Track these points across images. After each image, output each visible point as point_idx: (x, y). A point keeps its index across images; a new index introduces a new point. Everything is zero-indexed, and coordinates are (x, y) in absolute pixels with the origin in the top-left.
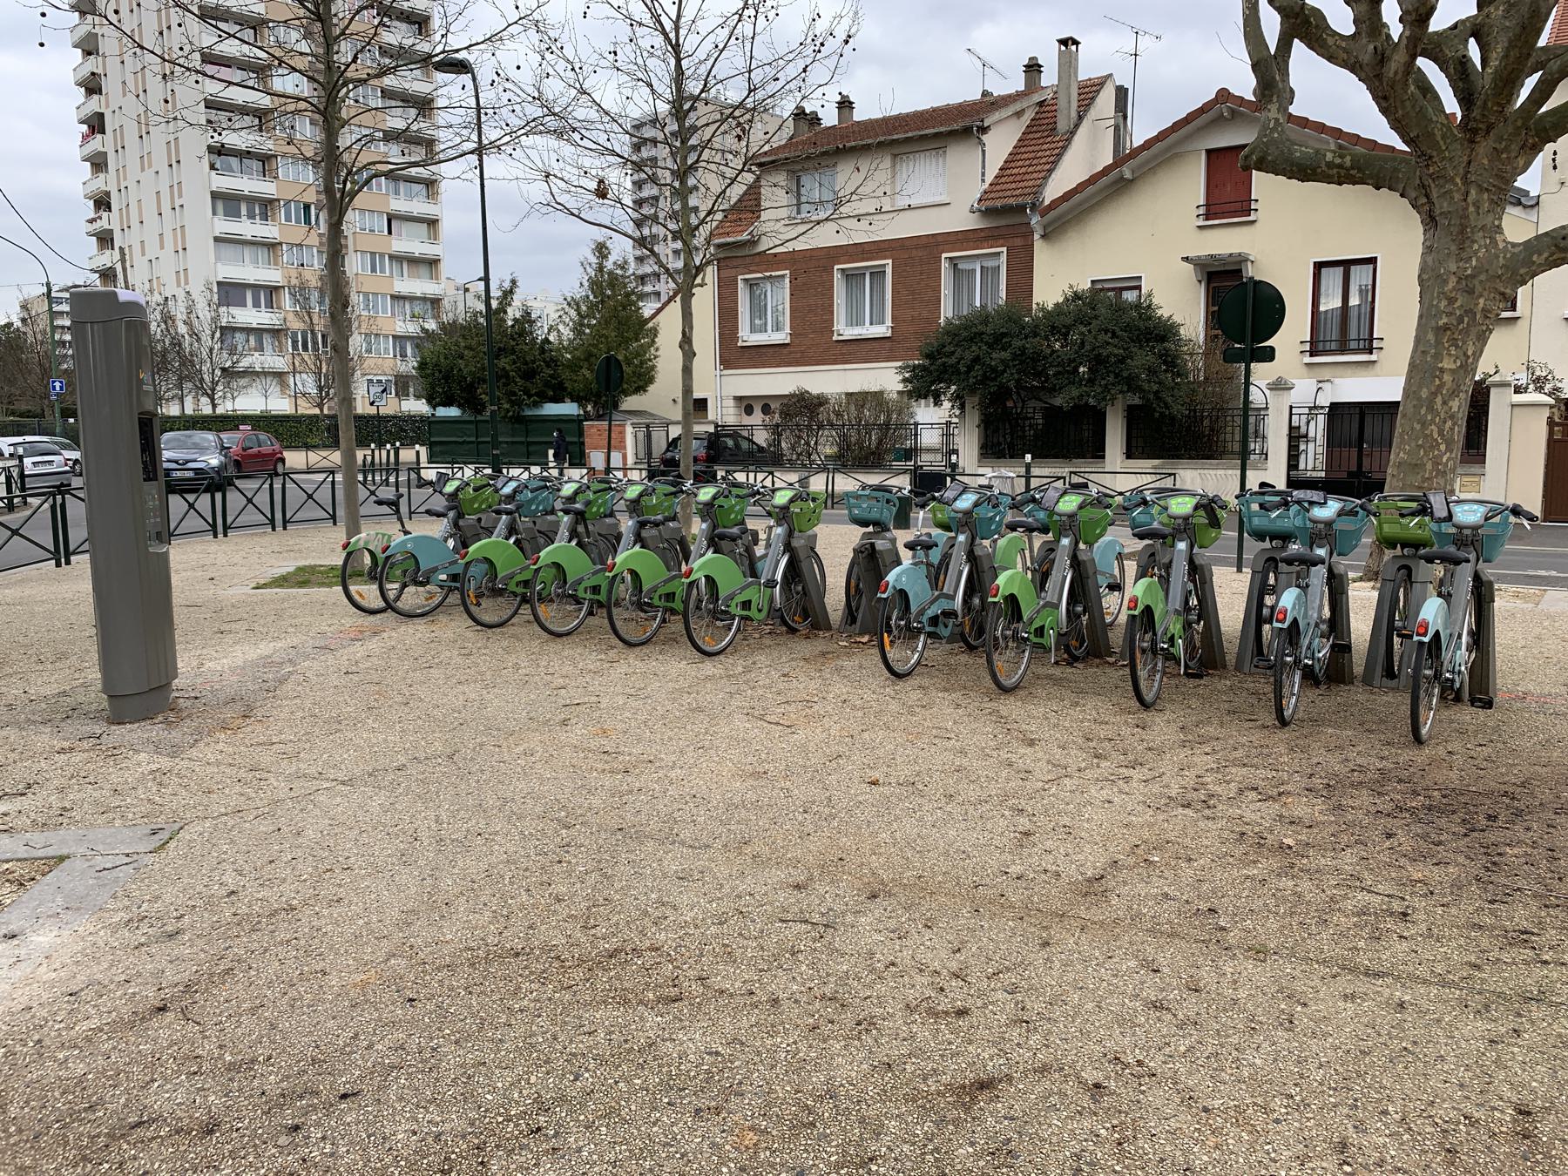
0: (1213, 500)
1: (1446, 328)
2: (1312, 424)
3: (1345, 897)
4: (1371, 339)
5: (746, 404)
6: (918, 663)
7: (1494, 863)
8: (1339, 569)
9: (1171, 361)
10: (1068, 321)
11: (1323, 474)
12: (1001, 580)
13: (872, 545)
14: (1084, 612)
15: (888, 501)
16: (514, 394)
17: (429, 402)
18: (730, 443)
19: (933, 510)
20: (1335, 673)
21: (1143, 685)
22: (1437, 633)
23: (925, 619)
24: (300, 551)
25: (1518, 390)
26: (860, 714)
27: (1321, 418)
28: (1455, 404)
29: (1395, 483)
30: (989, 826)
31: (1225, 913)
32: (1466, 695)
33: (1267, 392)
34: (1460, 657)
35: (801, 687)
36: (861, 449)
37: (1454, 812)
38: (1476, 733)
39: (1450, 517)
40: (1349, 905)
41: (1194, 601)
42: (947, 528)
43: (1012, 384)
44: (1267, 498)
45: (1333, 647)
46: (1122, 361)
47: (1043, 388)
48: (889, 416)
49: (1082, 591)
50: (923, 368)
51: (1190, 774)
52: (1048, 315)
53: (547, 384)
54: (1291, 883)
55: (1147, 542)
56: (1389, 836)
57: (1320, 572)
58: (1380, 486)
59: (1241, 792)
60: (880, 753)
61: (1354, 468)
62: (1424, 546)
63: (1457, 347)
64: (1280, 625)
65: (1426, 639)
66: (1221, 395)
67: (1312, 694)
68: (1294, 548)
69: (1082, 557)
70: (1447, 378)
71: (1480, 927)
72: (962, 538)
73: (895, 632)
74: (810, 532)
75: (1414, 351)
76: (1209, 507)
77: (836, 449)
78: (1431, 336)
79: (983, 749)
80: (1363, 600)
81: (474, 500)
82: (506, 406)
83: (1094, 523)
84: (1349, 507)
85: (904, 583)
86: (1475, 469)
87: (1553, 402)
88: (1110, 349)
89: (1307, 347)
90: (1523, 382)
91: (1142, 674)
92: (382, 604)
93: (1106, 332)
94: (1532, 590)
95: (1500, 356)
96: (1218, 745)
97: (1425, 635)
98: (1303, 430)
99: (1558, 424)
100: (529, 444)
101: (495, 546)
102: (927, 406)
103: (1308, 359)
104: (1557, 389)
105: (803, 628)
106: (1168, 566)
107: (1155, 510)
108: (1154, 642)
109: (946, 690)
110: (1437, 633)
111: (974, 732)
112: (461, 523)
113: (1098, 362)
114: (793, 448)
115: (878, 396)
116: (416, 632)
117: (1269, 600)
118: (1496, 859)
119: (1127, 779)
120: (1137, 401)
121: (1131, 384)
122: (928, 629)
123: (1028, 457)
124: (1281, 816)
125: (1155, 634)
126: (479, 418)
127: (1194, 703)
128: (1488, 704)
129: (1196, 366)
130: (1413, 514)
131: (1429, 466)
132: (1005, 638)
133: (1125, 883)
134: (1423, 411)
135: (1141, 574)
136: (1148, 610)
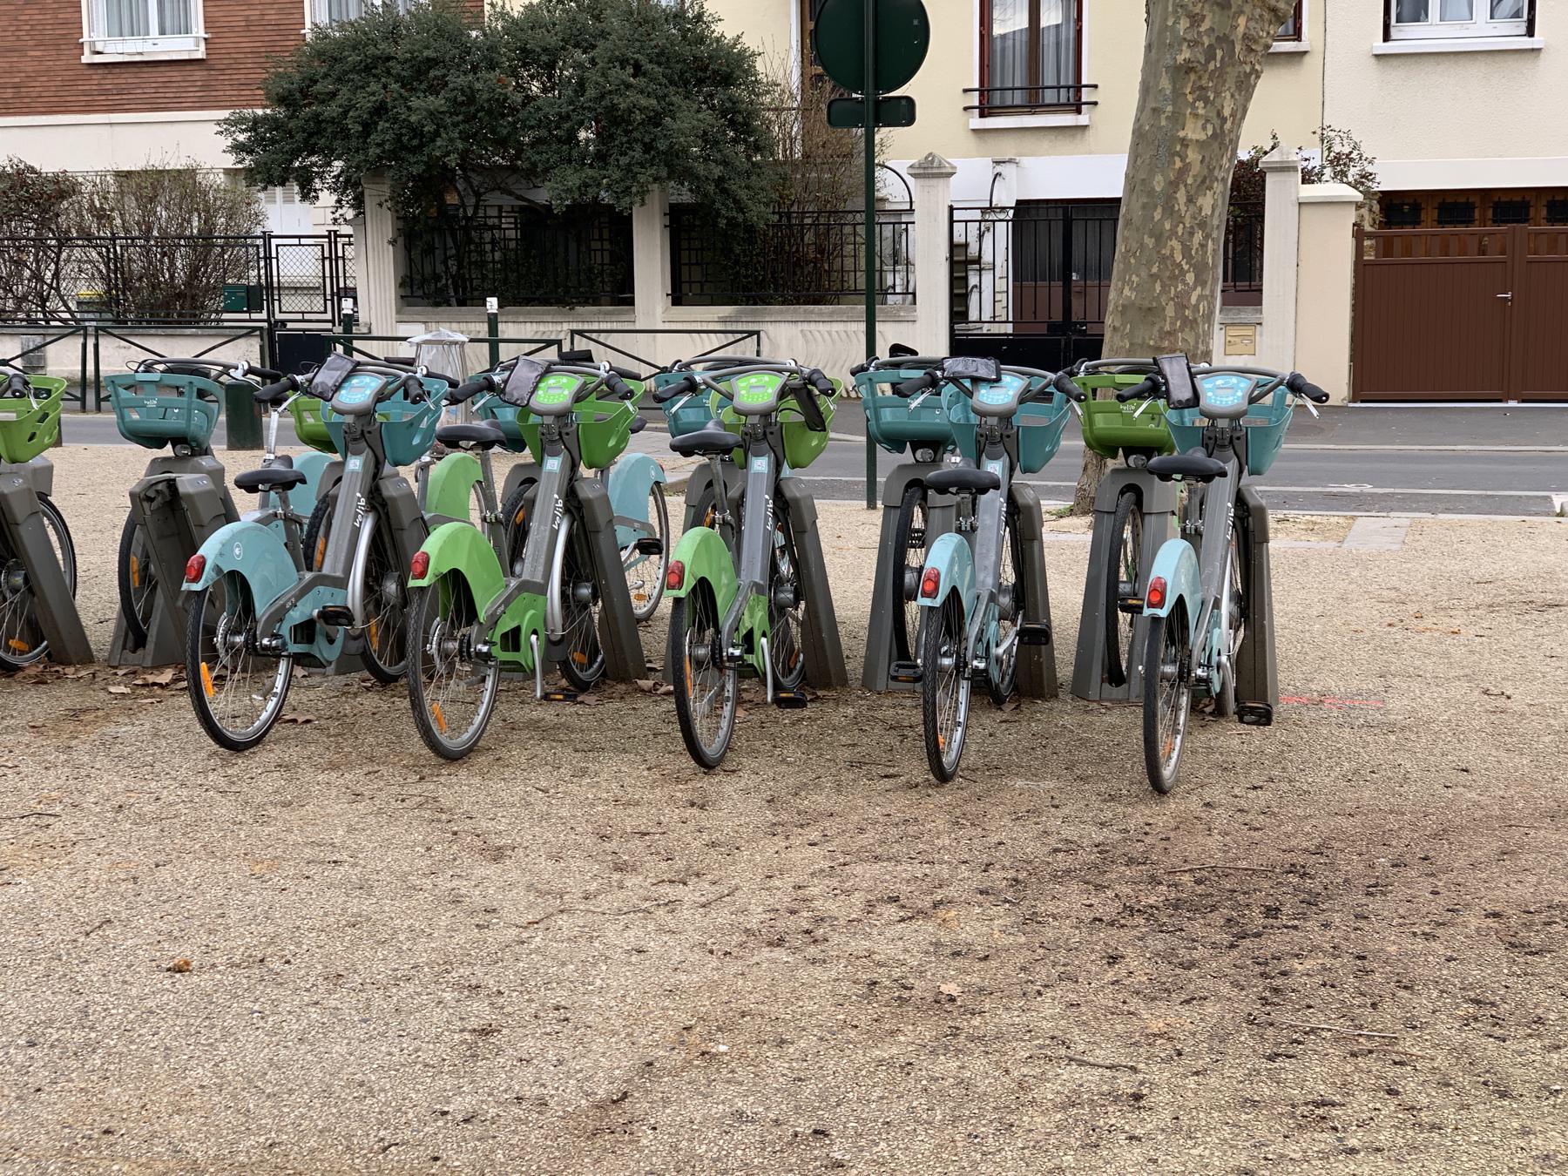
0: (809, 380)
1: (1188, 68)
2: (988, 238)
3: (1042, 1078)
4: (1078, 87)
6: (277, 717)
7: (1276, 990)
8: (1026, 497)
9: (742, 123)
10: (553, 41)
11: (1009, 328)
12: (432, 545)
13: (171, 484)
14: (595, 597)
15: (201, 394)
19: (296, 411)
20: (1024, 683)
21: (700, 727)
22: (1181, 600)
23: (285, 630)
25: (1308, 177)
26: (153, 831)
27: (1001, 228)
28: (1206, 202)
29: (1118, 343)
30: (413, 1025)
31: (842, 1135)
32: (1232, 706)
33: (911, 181)
34: (1219, 639)
35: (25, 786)
36: (154, 287)
37: (1214, 908)
38: (1247, 768)
39: (1195, 400)
40: (1047, 1092)
41: (785, 568)
42: (325, 444)
43: (452, 161)
44: (904, 373)
45: (1021, 634)
46: (655, 120)
47: (513, 169)
48: (208, 221)
49: (587, 559)
50: (273, 123)
51: (784, 883)
52: (513, 26)
54: (954, 1065)
55: (698, 460)
56: (1113, 960)
57: (993, 505)
58: (1093, 349)
59: (870, 907)
60: (195, 906)
61: (1058, 317)
62: (1160, 450)
63: (1206, 101)
64: (928, 602)
65: (1163, 613)
66: (834, 186)
67: (991, 720)
68: (954, 461)
69: (585, 492)
70: (1193, 156)
71: (1255, 1104)
72: (355, 464)
73: (225, 659)
74: (35, 462)
75: (1141, 108)
76: (805, 391)
77: (100, 288)
78: (1165, 83)
79: (404, 878)
80: (1067, 547)
83: (604, 427)
84: (1038, 385)
85: (238, 560)
86: (1247, 314)
87: (1359, 197)
88: (633, 97)
89: (974, 99)
90: (1316, 163)
91: (699, 708)
93: (624, 63)
94: (1334, 518)
95: (1274, 119)
96: (832, 827)
97: (1161, 605)
98: (973, 250)
99: (1370, 236)
102: (288, 200)
103: (977, 122)
104: (1366, 176)
105: (30, 662)
106: (738, 505)
107: (712, 399)
108: (717, 648)
109: (333, 767)
110: (1181, 600)
111: (387, 844)
113: (613, 123)
115: (185, 179)
117: (914, 558)
118: (1278, 982)
119: (672, 905)
120: (686, 197)
121: (674, 165)
122: (294, 648)
123: (492, 304)
124: (937, 944)
125: (718, 632)
127: (792, 752)
128: (1264, 718)
129: (788, 132)
130: (1139, 395)
131: (1170, 311)
132: (445, 655)
133: (666, 1102)
134: (1157, 216)
135: (695, 520)
136: (704, 589)
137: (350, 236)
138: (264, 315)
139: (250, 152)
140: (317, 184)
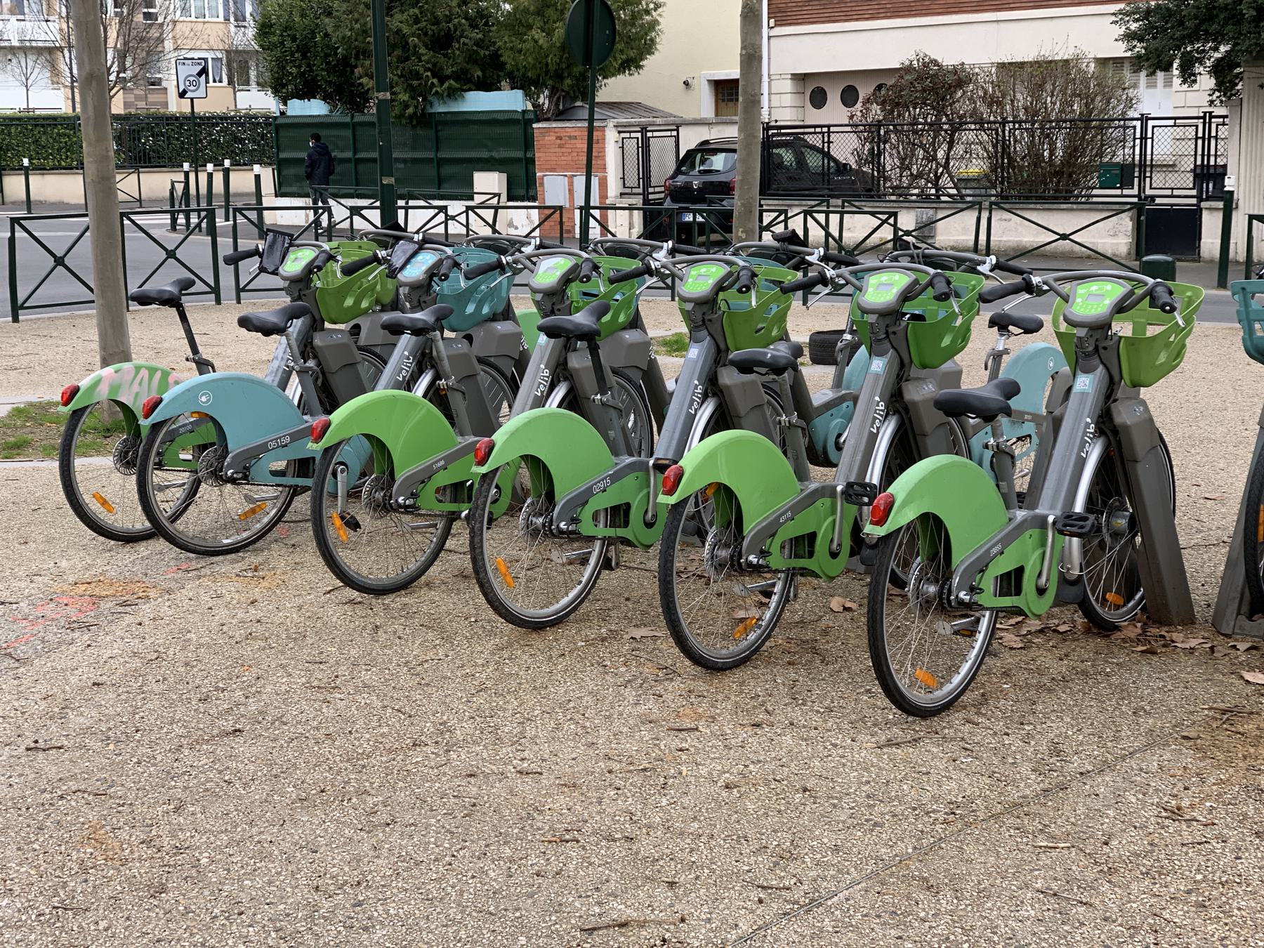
5: (814, 88)
16: (418, 76)
17: (276, 92)
18: (787, 156)
24: (29, 369)
53: (472, 58)
81: (342, 291)
82: (404, 97)
92: (140, 523)
100: (441, 162)
101: (389, 407)
112: (318, 341)
114: (904, 167)
116: (218, 595)
126: (359, 118)
137: (1224, 117)
138: (1135, 191)
139: (1141, 40)
140: (1198, 69)
